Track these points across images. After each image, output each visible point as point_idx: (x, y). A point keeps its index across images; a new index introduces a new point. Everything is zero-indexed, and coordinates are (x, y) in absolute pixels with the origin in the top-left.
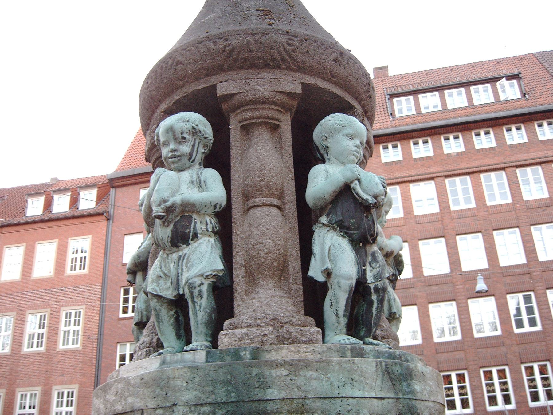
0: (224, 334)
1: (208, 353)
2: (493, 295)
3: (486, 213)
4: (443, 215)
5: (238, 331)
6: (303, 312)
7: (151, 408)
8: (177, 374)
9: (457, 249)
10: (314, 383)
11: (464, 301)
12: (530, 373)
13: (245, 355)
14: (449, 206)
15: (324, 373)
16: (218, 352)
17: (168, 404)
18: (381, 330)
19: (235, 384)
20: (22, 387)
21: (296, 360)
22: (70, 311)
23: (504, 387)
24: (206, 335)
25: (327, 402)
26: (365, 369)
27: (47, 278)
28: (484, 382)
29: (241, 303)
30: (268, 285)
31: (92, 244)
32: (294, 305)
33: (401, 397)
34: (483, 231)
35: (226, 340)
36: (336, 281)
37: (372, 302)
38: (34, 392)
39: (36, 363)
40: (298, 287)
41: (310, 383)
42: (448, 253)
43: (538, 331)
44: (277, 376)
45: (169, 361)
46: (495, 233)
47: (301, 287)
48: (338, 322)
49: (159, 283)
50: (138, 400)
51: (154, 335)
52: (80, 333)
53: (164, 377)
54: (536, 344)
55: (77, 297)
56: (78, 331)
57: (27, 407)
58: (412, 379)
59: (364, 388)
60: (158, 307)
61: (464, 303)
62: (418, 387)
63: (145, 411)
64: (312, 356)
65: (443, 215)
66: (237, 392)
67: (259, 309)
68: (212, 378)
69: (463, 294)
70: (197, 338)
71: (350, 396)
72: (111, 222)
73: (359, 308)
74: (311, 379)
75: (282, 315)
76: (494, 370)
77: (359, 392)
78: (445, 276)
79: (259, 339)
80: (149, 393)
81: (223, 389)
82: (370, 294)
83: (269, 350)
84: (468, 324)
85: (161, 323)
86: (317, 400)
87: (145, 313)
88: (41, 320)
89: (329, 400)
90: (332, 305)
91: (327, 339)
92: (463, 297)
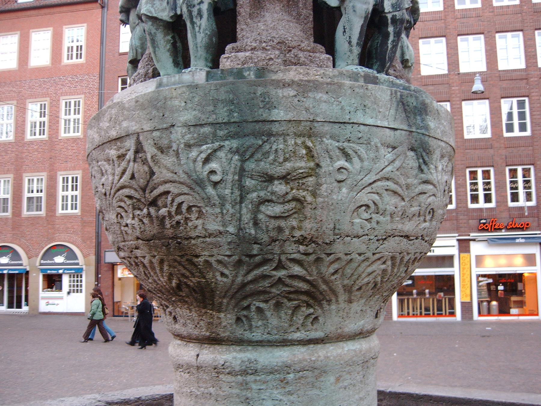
0: (225, 58)
1: (208, 73)
2: (488, 99)
3: (491, 14)
4: (447, 13)
5: (241, 55)
6: (312, 39)
7: (148, 131)
8: (174, 94)
9: (457, 50)
10: (324, 106)
11: (458, 102)
12: (513, 175)
13: (249, 75)
14: (454, 4)
15: (334, 96)
16: (220, 72)
17: (165, 126)
18: (394, 70)
19: (238, 104)
20: (28, 172)
21: (306, 81)
22: (70, 100)
23: (487, 187)
24: (206, 59)
25: (336, 127)
26: (379, 96)
27: (44, 68)
28: (468, 182)
29: (245, 27)
30: (274, 8)
31: (88, 32)
32: (303, 31)
33: (414, 130)
34: (486, 32)
35: (228, 63)
36: (351, 4)
37: (387, 35)
38: (40, 177)
39: (40, 150)
40: (308, 12)
41: (319, 106)
42: (448, 54)
43: (527, 136)
44: (284, 96)
45: (166, 83)
46: (497, 35)
47: (312, 13)
48: (351, 51)
49: (154, 4)
50: (134, 123)
51: (149, 66)
52: (80, 122)
53: (161, 97)
54: (523, 148)
55: (76, 87)
56: (78, 119)
57: (35, 191)
58: (427, 115)
59: (377, 116)
60: (153, 31)
61: (458, 104)
62: (432, 124)
63: (140, 134)
64: (322, 79)
65: (447, 13)
66: (240, 111)
67: (265, 33)
68: (213, 97)
69: (458, 95)
70: (196, 63)
71: (361, 122)
72: (106, 9)
73: (373, 41)
74: (320, 101)
75: (290, 39)
76: (480, 171)
77: (371, 120)
78: (444, 75)
79: (265, 63)
80: (145, 116)
81: (225, 109)
82: (387, 26)
83: (275, 70)
84: (460, 125)
85: (157, 49)
86: (326, 124)
87: (140, 50)
88: (41, 109)
89: (340, 125)
90: (345, 31)
91: (337, 64)
92: (458, 99)
